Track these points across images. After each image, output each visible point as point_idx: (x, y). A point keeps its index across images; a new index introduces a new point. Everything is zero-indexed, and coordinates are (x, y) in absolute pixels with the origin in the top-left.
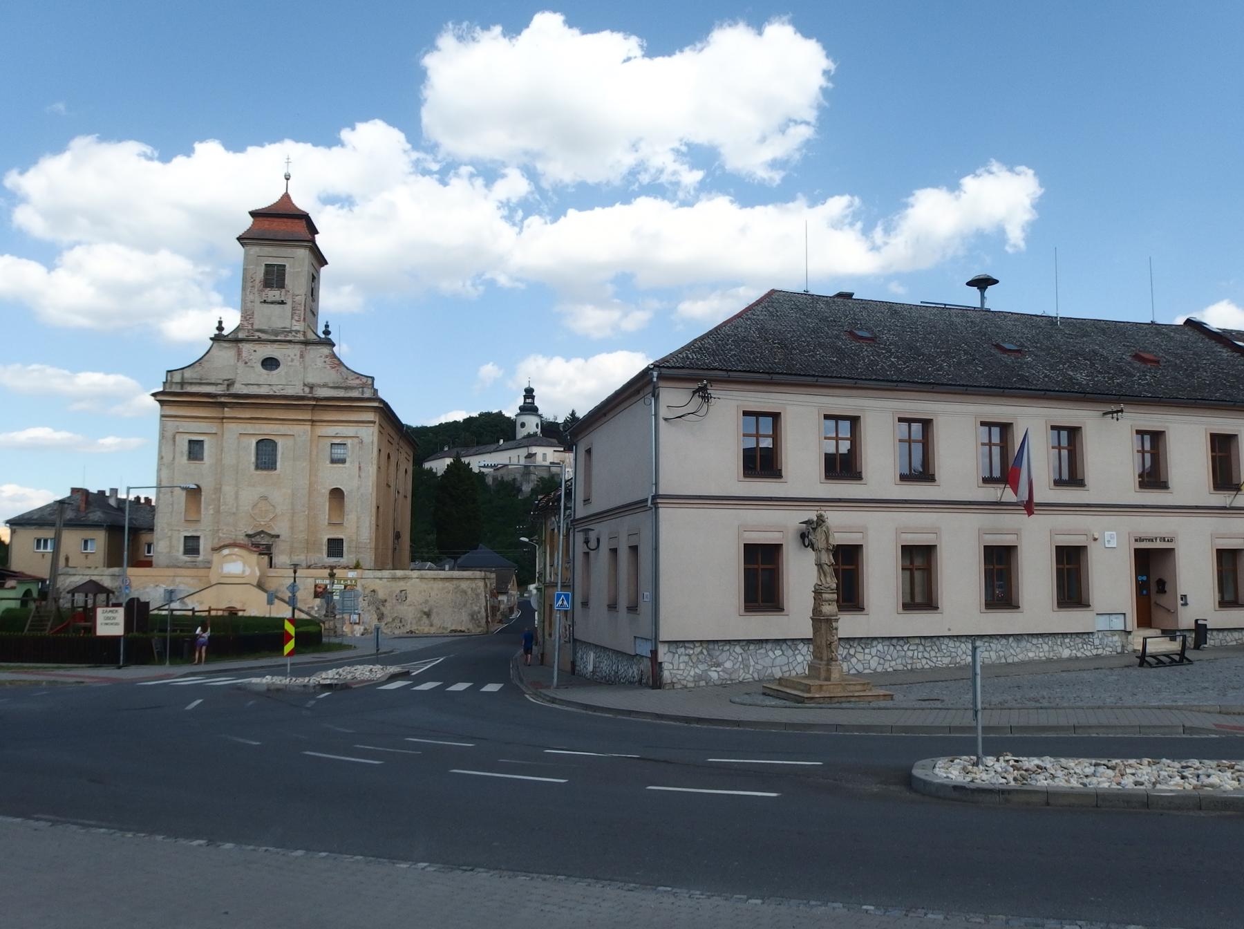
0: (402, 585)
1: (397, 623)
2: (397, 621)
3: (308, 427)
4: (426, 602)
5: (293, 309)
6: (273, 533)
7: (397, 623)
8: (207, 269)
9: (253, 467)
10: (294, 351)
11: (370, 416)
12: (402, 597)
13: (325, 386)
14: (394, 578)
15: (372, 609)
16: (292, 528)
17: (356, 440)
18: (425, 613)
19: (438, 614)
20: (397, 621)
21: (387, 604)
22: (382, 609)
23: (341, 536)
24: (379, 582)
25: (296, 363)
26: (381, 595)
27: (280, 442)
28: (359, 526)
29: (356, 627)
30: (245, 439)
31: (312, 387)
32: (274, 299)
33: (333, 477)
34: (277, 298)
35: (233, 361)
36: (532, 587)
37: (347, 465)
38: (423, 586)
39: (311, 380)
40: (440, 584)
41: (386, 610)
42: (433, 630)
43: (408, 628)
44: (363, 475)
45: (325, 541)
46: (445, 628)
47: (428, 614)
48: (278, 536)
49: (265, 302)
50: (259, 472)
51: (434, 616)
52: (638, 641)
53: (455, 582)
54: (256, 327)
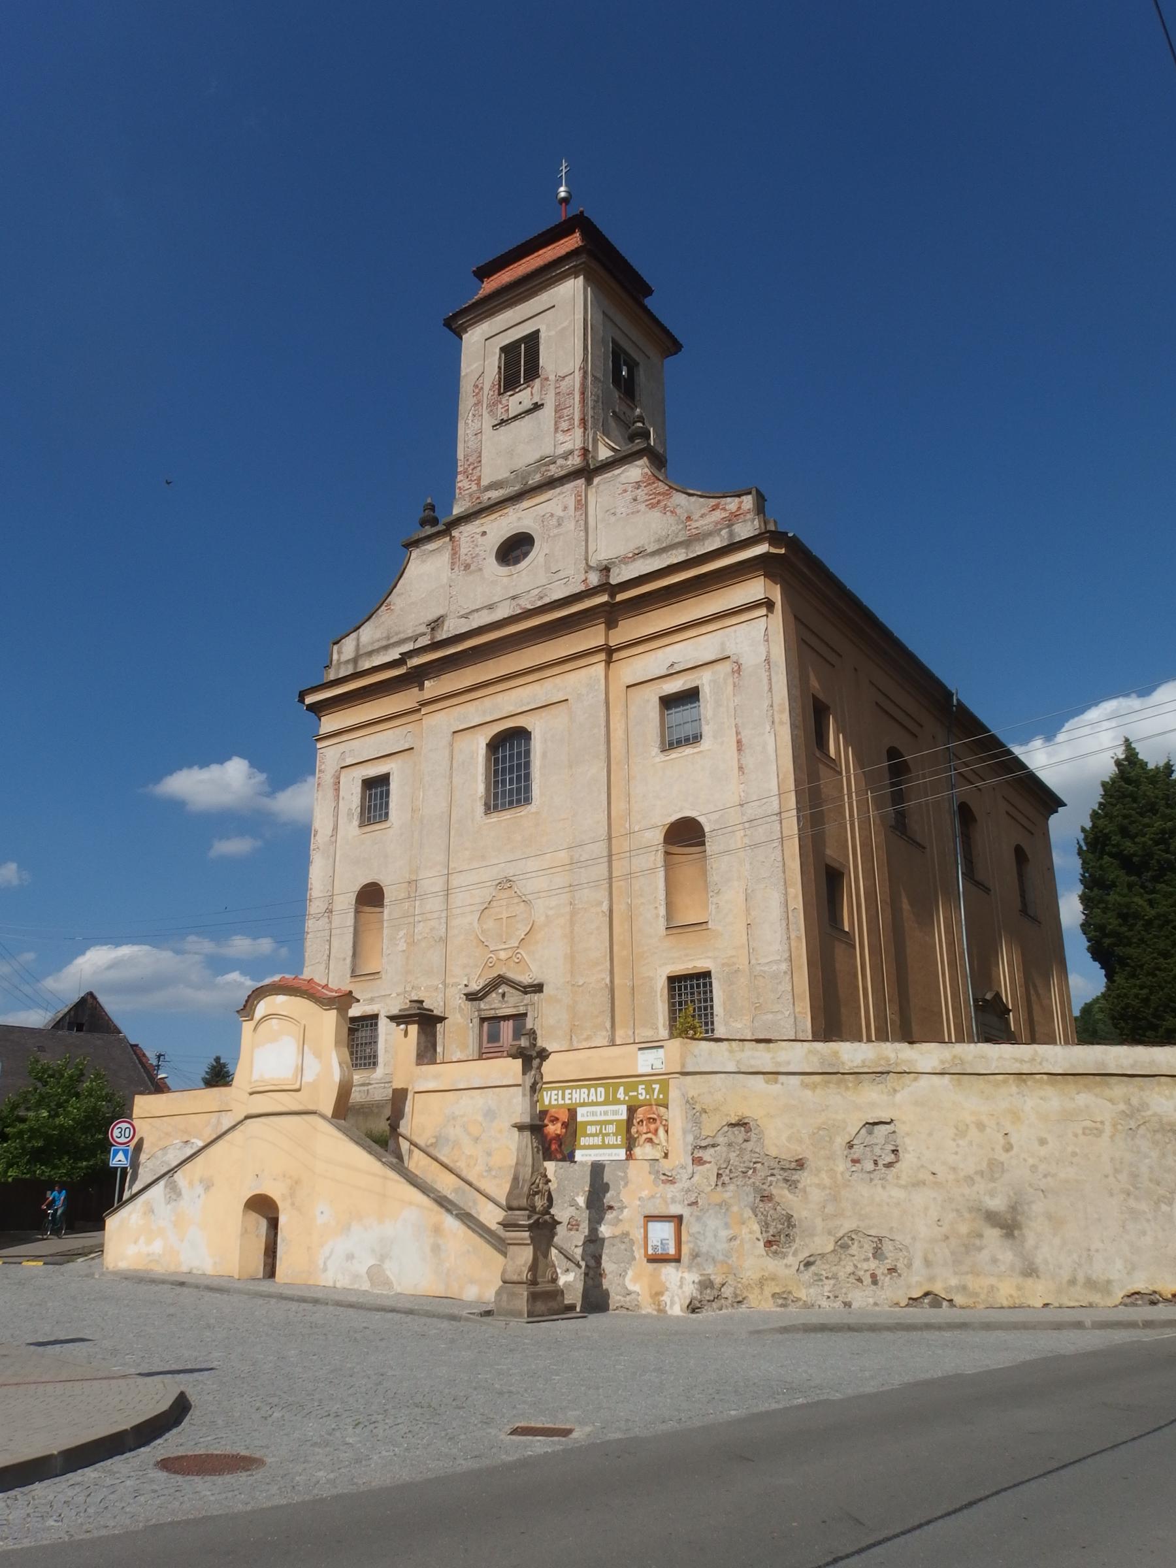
0: (873, 1100)
1: (860, 1258)
2: (861, 1250)
3: (596, 670)
4: (994, 1170)
5: (558, 409)
6: (525, 979)
7: (860, 1258)
8: (1085, 848)
9: (480, 808)
10: (560, 501)
11: (755, 588)
12: (876, 1149)
13: (640, 554)
14: (832, 1074)
15: (739, 1197)
16: (572, 958)
17: (725, 668)
18: (992, 1218)
19: (1056, 1222)
20: (861, 1250)
21: (805, 1178)
22: (781, 1192)
23: (701, 965)
24: (778, 1080)
25: (570, 525)
26: (778, 1139)
27: (536, 725)
28: (755, 921)
29: (669, 1273)
30: (463, 742)
31: (606, 570)
32: (521, 409)
33: (672, 786)
34: (528, 404)
35: (446, 574)
36: (563, 195)
37: (706, 744)
38: (970, 1103)
39: (603, 552)
40: (1053, 1099)
41: (805, 1203)
42: (1038, 1293)
43: (915, 1282)
44: (749, 761)
45: (661, 984)
46: (1105, 1287)
47: (1008, 1225)
48: (538, 988)
49: (503, 422)
50: (495, 818)
51: (1035, 1231)
52: (297, 1086)
53: (1119, 1089)
54: (484, 483)
